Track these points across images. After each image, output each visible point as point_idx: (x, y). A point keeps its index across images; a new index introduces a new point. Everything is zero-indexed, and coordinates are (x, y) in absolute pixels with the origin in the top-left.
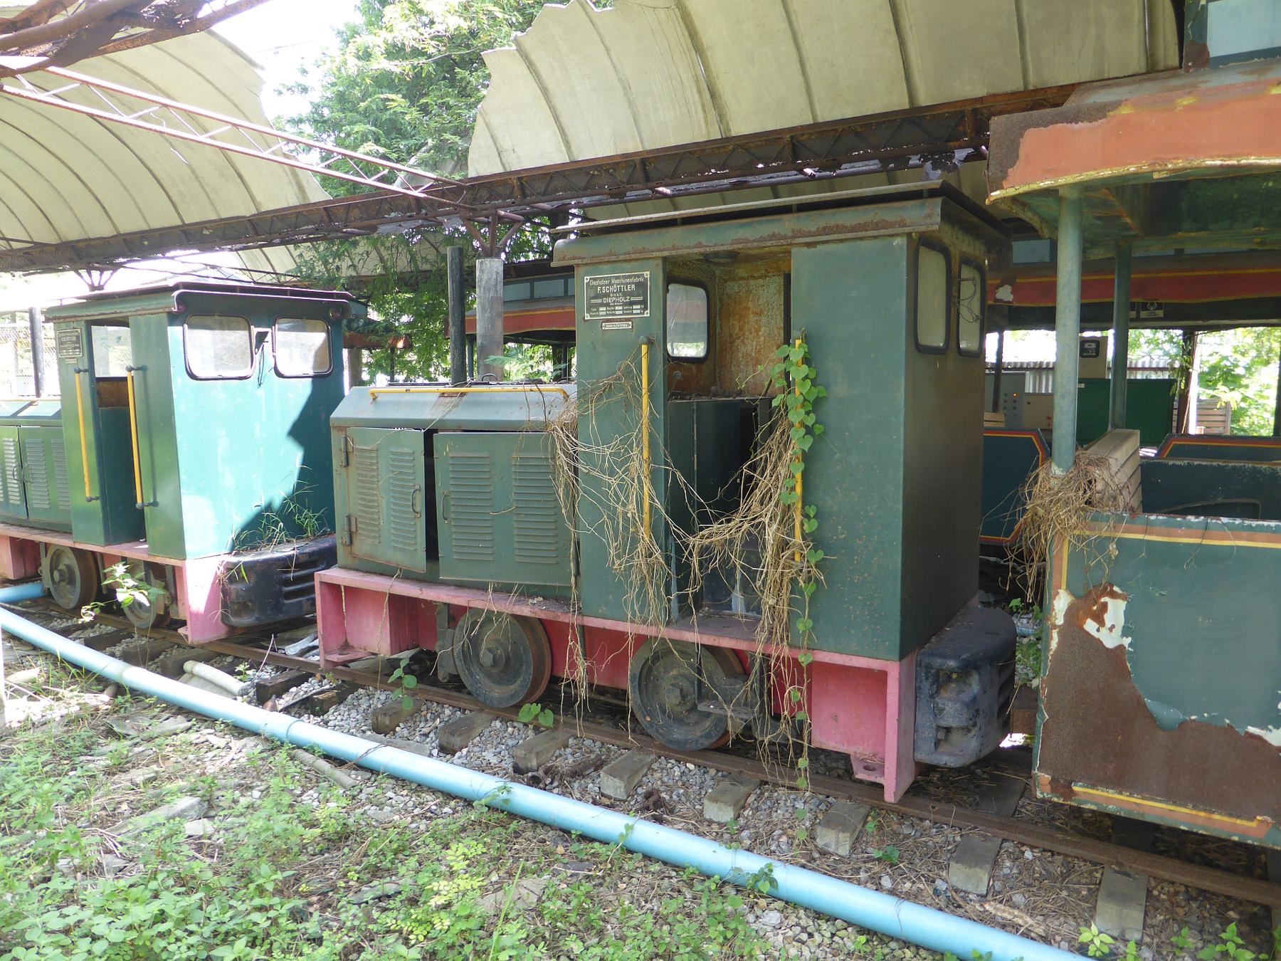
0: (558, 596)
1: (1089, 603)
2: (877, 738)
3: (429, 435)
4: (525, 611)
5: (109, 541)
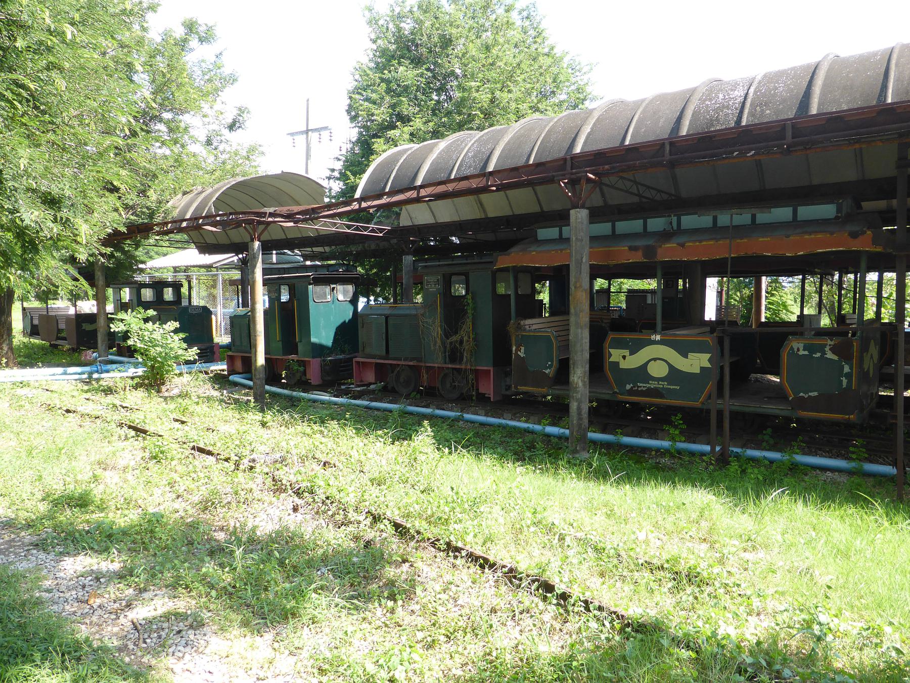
0: (419, 360)
1: (518, 349)
2: (488, 388)
3: (387, 318)
4: (411, 363)
5: (284, 355)
